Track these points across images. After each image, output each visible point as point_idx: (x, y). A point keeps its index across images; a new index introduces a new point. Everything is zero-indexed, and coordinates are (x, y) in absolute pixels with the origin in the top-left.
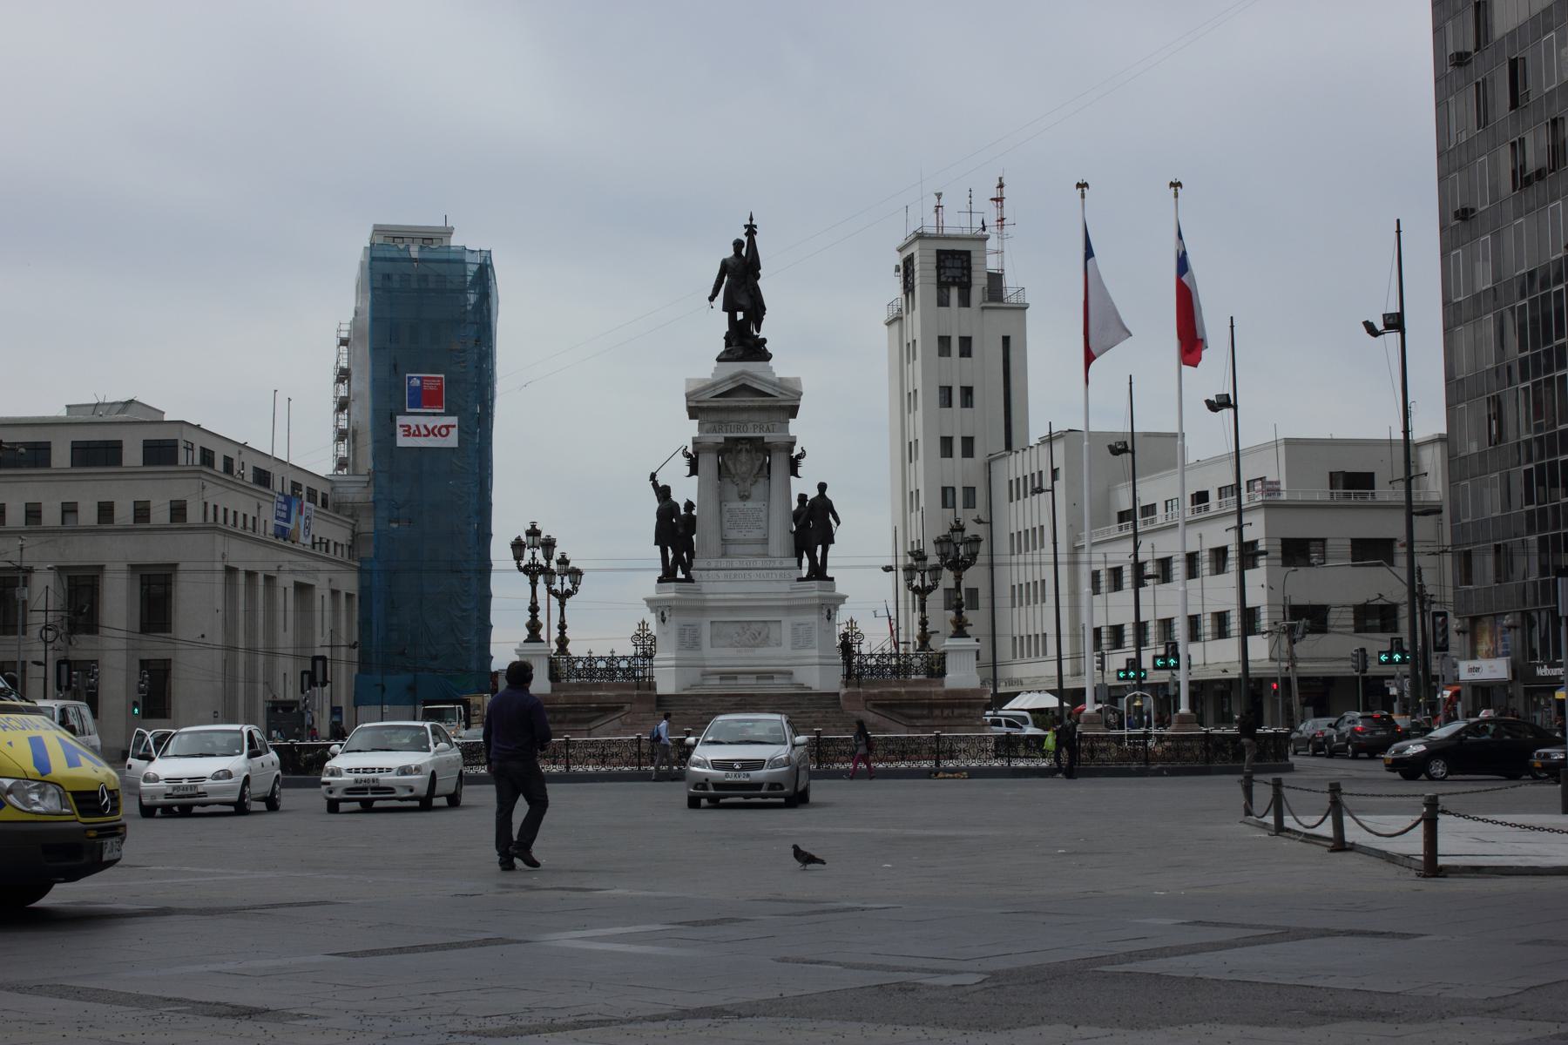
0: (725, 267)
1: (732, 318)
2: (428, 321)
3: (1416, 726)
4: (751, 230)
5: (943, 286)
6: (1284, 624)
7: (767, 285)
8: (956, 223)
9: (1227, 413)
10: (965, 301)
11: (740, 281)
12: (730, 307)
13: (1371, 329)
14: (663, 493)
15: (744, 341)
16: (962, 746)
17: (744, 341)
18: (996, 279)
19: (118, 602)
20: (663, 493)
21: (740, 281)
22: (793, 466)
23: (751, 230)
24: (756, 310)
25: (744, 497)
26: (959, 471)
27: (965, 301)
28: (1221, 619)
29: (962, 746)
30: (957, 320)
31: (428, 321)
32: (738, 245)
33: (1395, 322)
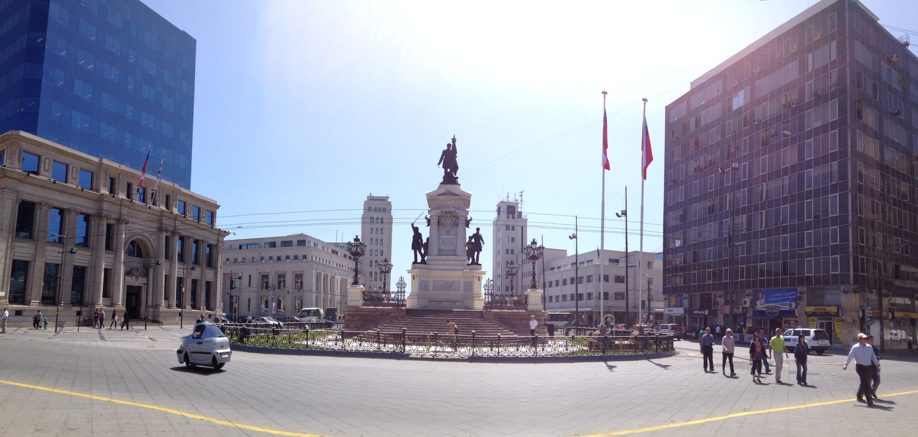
0: (444, 153)
1: (446, 171)
2: (378, 212)
3: (326, 323)
4: (454, 140)
5: (508, 213)
6: (535, 297)
7: (459, 160)
8: (512, 200)
9: (574, 240)
10: (513, 218)
11: (449, 159)
12: (445, 167)
13: (617, 215)
14: (416, 230)
15: (450, 178)
16: (296, 336)
17: (450, 178)
18: (520, 213)
19: (290, 280)
20: (416, 230)
21: (449, 159)
22: (467, 223)
23: (454, 140)
24: (455, 168)
25: (448, 233)
26: (510, 257)
27: (513, 218)
28: (551, 286)
29: (296, 336)
30: (511, 222)
31: (378, 212)
32: (449, 145)
33: (625, 213)
